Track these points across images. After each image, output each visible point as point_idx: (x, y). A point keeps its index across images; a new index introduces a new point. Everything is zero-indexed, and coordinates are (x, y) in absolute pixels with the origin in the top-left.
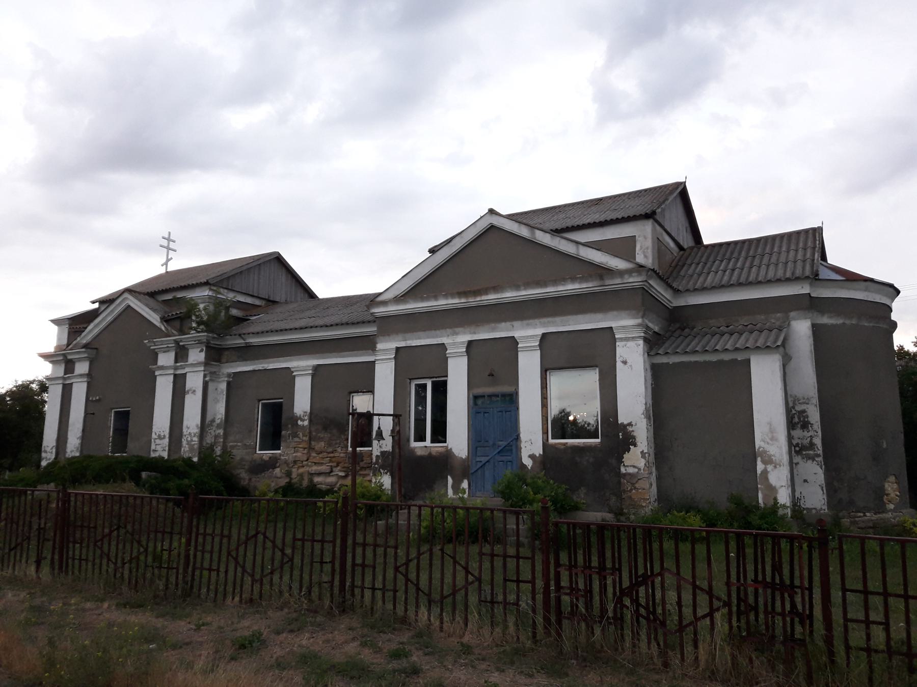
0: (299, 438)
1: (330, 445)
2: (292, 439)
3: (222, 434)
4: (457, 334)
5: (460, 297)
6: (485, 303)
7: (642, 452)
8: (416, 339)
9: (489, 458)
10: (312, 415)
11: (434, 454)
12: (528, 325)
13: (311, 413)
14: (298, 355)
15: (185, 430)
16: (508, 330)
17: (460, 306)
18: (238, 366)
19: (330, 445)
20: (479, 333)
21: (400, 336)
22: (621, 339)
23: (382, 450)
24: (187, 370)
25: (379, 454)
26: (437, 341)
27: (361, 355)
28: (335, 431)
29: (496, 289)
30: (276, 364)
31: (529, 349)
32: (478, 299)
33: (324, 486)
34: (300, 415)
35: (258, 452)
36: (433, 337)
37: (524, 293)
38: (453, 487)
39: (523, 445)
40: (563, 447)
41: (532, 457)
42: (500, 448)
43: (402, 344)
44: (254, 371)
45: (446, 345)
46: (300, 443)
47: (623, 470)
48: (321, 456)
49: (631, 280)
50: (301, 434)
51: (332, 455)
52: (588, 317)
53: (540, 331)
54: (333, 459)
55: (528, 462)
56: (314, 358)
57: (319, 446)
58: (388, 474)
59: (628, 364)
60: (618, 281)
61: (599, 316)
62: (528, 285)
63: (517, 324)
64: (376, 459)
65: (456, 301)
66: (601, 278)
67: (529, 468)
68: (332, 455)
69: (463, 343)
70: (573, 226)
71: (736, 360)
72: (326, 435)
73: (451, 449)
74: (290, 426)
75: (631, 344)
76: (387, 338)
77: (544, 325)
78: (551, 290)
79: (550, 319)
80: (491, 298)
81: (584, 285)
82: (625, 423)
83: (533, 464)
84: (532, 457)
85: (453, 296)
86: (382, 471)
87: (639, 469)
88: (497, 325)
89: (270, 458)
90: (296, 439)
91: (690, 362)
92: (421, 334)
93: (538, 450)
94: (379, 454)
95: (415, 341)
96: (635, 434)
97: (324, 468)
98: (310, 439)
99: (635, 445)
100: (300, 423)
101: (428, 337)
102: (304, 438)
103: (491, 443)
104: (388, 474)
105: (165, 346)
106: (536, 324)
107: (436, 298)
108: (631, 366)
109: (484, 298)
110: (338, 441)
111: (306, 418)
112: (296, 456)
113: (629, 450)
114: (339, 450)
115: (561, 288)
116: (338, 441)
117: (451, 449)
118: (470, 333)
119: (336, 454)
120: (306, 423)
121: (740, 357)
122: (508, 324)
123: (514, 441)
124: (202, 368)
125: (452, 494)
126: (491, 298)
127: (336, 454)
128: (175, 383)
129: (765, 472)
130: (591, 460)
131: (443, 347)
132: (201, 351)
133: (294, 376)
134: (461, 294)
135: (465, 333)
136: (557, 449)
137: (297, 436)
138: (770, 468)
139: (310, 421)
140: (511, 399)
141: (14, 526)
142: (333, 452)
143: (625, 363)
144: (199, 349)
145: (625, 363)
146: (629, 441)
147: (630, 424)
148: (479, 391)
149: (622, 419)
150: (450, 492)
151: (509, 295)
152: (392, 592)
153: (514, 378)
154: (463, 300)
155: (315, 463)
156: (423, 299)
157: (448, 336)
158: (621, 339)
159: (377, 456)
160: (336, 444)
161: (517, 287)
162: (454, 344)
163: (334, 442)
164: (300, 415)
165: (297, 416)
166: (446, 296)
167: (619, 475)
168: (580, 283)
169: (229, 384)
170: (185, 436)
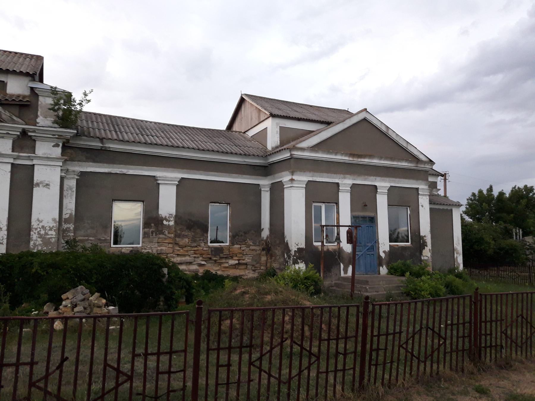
0: (165, 235)
1: (194, 241)
2: (156, 235)
3: (72, 228)
4: (345, 178)
5: (349, 157)
6: (361, 163)
7: (429, 250)
8: (320, 177)
9: (362, 252)
10: (178, 218)
11: (331, 250)
12: (383, 180)
13: (176, 216)
14: (164, 167)
15: (34, 223)
16: (372, 181)
17: (347, 162)
18: (90, 166)
19: (194, 241)
20: (357, 180)
21: (311, 174)
22: (422, 195)
23: (299, 247)
24: (35, 162)
25: (296, 250)
26: (332, 181)
27: (223, 177)
28: (198, 231)
29: (371, 156)
30: (137, 171)
31: (382, 193)
32: (359, 160)
33: (188, 273)
34: (166, 217)
35: (112, 246)
36: (330, 178)
37: (382, 162)
38: (343, 270)
39: (380, 246)
40: (397, 247)
41: (384, 252)
42: (368, 248)
43: (311, 179)
44: (110, 174)
45: (340, 184)
46: (165, 239)
47: (422, 258)
48: (185, 249)
49: (427, 167)
50: (167, 232)
51: (196, 249)
52: (406, 181)
53: (388, 185)
54: (197, 252)
55: (383, 255)
56: (179, 172)
57: (184, 241)
58: (304, 263)
59: (424, 207)
60: (422, 166)
61: (414, 181)
62: (387, 158)
63: (378, 178)
64: (294, 253)
65: (347, 158)
66: (417, 163)
67: (383, 258)
68: (196, 249)
69: (349, 184)
70: (309, 119)
71: (448, 209)
72: (190, 234)
73: (342, 247)
74: (153, 225)
75: (424, 197)
76: (302, 173)
77: (390, 182)
78: (395, 164)
79: (394, 179)
80: (366, 161)
81: (410, 165)
82: (423, 235)
83: (385, 256)
84: (384, 252)
85: (346, 154)
86: (299, 261)
87: (429, 258)
88: (369, 177)
89: (131, 251)
90: (161, 236)
91: (436, 208)
92: (325, 174)
93: (387, 249)
94: (296, 250)
95: (318, 178)
96: (426, 241)
97: (187, 259)
98: (176, 236)
99: (427, 246)
100: (165, 222)
101: (328, 177)
102: (170, 235)
103: (363, 244)
104: (304, 263)
105: (5, 132)
106: (387, 181)
107: (336, 154)
108: (425, 208)
109: (363, 160)
110: (202, 238)
111: (172, 219)
112: (161, 250)
113: (424, 248)
114: (203, 245)
115: (399, 164)
116: (202, 238)
117: (342, 247)
118: (353, 180)
119: (200, 248)
120: (172, 223)
121: (449, 208)
122: (342, 176)
123: (374, 244)
124: (61, 164)
125: (343, 274)
126: (366, 161)
127: (200, 248)
128: (12, 172)
129: (457, 257)
130: (409, 253)
131: (338, 184)
132: (57, 145)
133: (159, 184)
134: (353, 155)
135: (349, 179)
136: (394, 248)
137: (163, 233)
138: (458, 255)
139: (176, 222)
140: (373, 220)
141: (430, 325)
142: (196, 247)
143: (422, 206)
144: (53, 144)
145: (422, 206)
146: (423, 245)
147: (425, 236)
148: (357, 214)
149: (422, 234)
150: (342, 272)
151: (375, 161)
152: (385, 336)
153: (375, 209)
154: (351, 159)
155: (178, 255)
156: (328, 152)
157: (340, 178)
158: (422, 195)
159: (295, 251)
160: (200, 240)
161: (381, 158)
162: (345, 184)
163: (198, 239)
164: (166, 217)
165: (162, 217)
166: (342, 154)
167: (421, 260)
168: (408, 163)
169: (78, 182)
170: (36, 229)
